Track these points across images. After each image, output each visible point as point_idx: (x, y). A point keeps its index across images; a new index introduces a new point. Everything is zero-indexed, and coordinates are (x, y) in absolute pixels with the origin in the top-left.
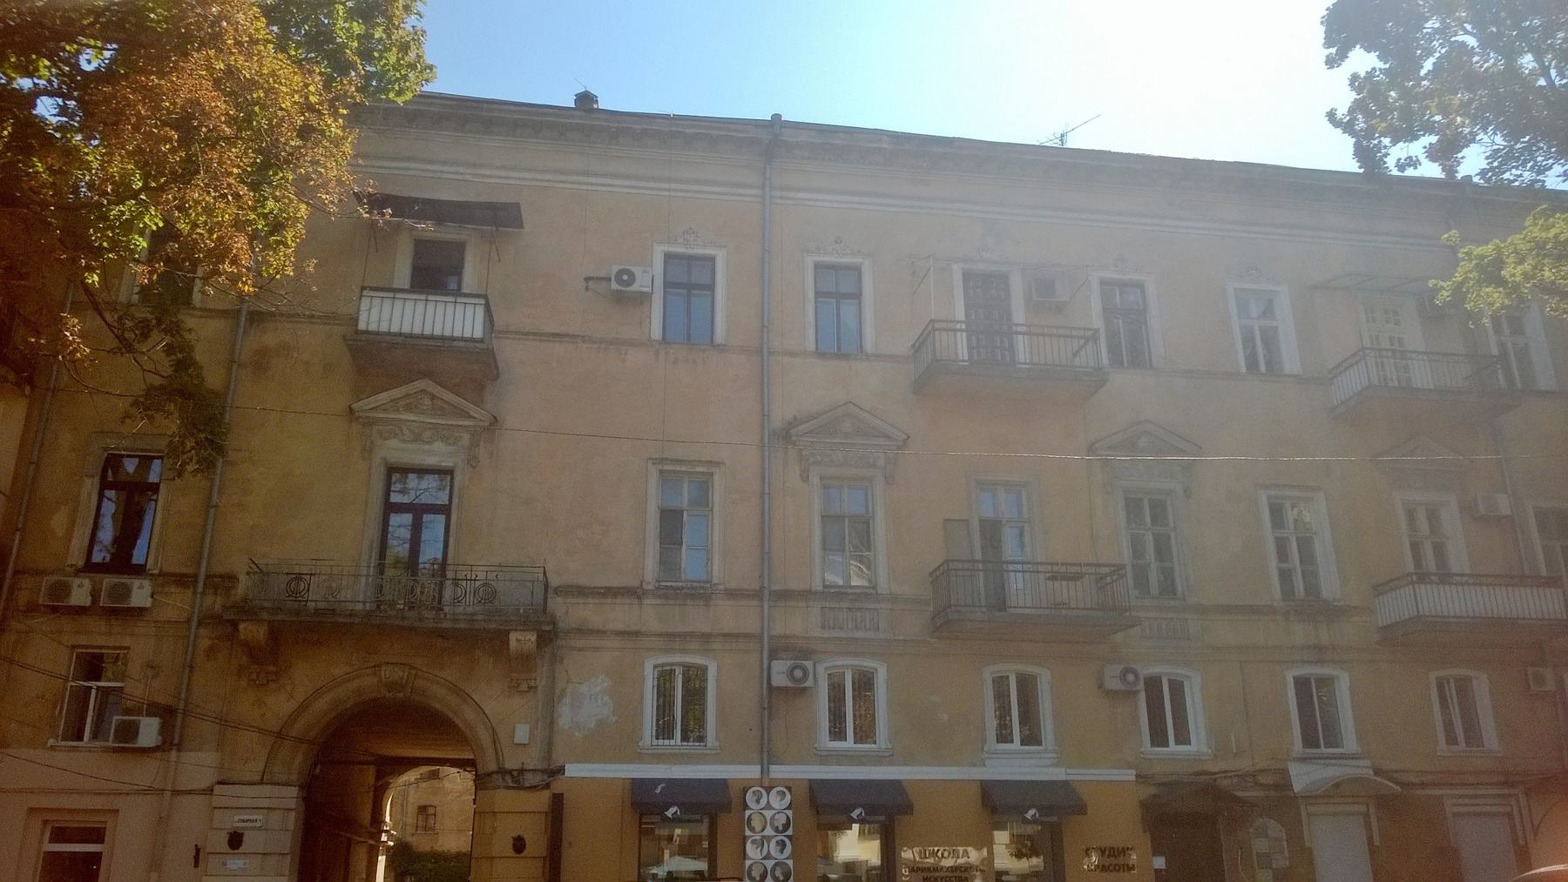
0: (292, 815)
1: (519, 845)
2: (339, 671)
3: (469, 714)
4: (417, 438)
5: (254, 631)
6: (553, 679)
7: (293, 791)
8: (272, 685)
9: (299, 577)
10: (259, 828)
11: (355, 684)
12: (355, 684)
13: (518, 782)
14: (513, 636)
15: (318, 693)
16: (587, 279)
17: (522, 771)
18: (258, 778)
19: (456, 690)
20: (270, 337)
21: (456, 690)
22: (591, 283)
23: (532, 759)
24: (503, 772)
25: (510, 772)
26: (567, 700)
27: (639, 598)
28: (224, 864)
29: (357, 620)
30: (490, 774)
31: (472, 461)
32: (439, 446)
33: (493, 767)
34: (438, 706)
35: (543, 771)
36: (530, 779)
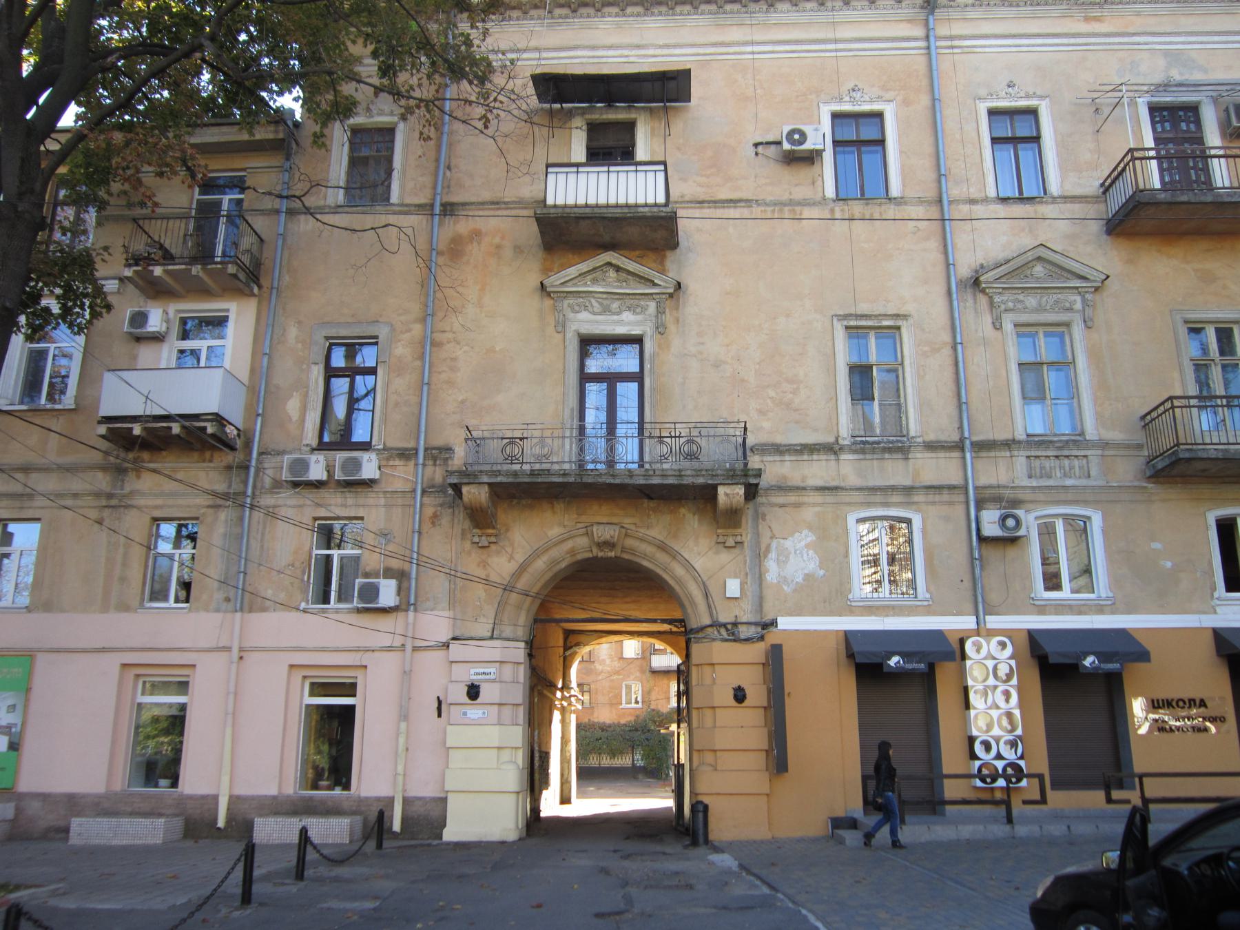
0: (522, 668)
1: (740, 695)
2: (555, 532)
3: (680, 571)
4: (606, 310)
5: (475, 494)
6: (757, 535)
7: (522, 645)
8: (493, 547)
9: (512, 441)
10: (494, 681)
11: (569, 545)
12: (569, 545)
13: (733, 634)
14: (721, 490)
15: (535, 555)
16: (756, 145)
17: (735, 624)
18: (489, 634)
19: (663, 547)
20: (462, 226)
21: (663, 547)
22: (760, 149)
23: (745, 613)
24: (716, 625)
25: (724, 625)
26: (773, 555)
27: (835, 453)
28: (465, 714)
29: (571, 480)
30: (702, 629)
31: (661, 329)
32: (627, 316)
33: (707, 621)
34: (645, 563)
35: (756, 624)
36: (744, 632)
